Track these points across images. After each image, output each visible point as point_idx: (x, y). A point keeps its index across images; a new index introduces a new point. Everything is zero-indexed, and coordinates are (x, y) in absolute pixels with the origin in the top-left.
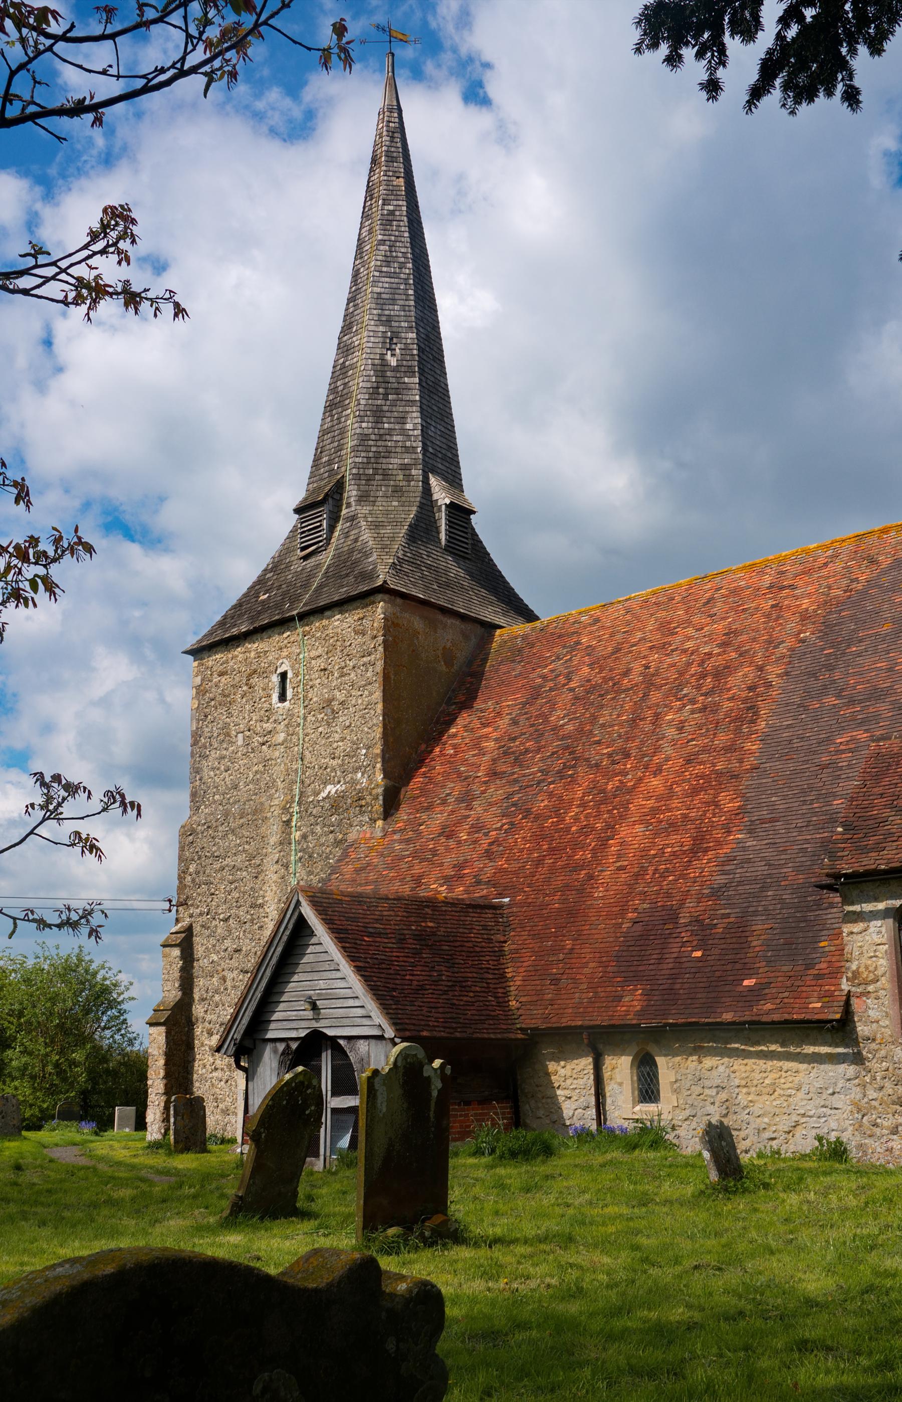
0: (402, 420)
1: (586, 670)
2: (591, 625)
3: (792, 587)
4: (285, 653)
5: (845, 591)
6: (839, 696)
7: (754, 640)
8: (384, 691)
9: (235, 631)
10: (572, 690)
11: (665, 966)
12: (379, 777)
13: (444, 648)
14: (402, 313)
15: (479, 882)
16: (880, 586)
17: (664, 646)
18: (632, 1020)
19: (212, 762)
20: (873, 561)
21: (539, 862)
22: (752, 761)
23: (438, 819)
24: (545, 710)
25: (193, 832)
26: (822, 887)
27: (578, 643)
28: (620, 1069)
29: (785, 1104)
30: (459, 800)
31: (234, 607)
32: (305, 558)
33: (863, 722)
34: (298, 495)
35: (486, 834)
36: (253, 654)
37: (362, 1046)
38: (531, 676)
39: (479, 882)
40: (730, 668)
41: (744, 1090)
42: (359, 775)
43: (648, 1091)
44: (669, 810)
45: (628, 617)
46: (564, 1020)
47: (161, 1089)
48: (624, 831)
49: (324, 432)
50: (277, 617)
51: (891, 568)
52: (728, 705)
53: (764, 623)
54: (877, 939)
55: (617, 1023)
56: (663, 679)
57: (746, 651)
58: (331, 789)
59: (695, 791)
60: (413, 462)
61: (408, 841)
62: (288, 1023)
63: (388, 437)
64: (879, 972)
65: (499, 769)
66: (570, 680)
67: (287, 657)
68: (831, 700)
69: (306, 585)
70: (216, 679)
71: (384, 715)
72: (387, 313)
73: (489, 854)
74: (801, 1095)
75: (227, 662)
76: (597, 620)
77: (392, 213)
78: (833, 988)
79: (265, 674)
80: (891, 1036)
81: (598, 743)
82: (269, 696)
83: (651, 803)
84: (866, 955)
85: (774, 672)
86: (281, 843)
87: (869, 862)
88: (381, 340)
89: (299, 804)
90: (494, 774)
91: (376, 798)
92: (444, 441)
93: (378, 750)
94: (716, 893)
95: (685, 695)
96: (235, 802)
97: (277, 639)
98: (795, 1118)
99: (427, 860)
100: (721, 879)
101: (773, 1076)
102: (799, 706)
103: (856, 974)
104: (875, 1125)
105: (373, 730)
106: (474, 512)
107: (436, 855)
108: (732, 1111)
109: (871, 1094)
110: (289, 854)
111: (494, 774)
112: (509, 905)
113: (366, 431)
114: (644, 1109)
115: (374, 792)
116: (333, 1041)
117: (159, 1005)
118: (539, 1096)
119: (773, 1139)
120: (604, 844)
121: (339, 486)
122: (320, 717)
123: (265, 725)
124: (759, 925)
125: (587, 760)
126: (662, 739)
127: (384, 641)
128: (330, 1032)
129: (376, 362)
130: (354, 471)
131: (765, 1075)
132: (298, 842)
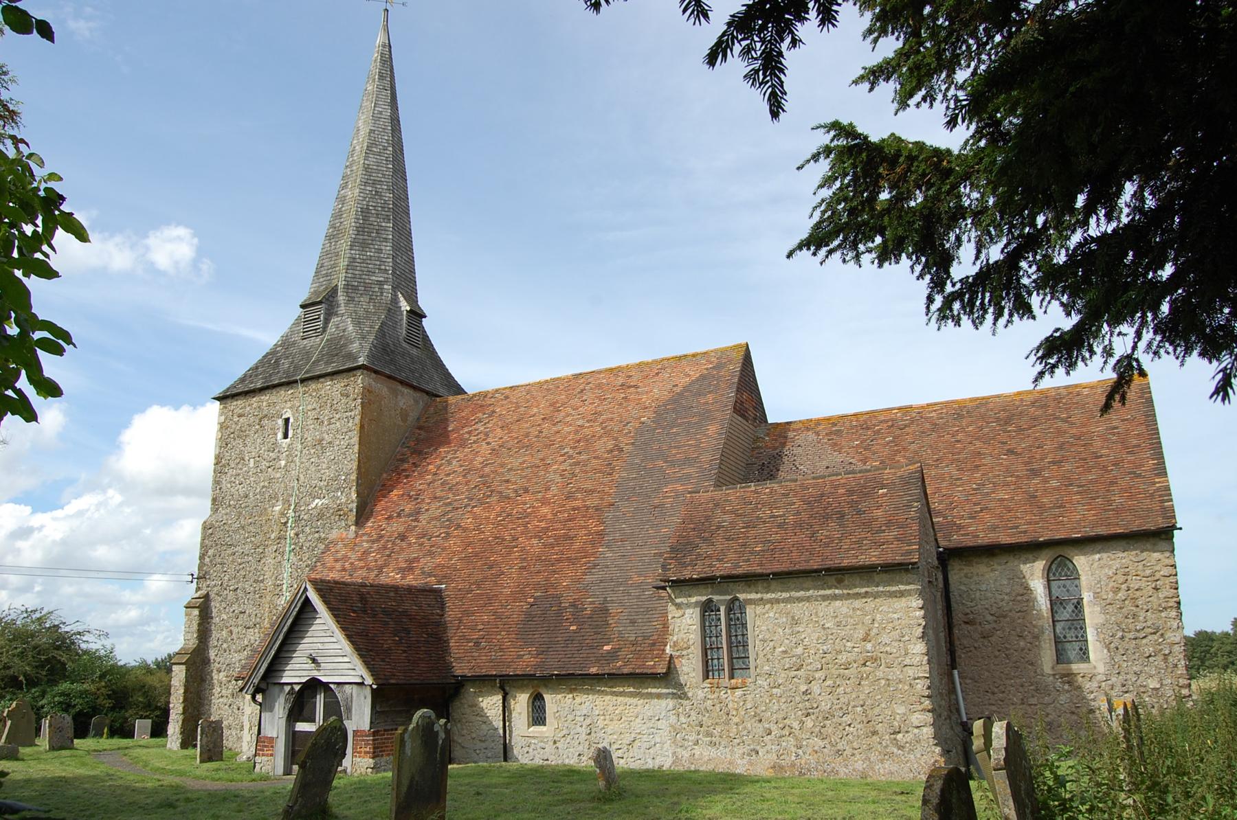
3: (636, 387)
4: (289, 405)
12: (354, 496)
26: (658, 588)
27: (494, 412)
28: (521, 702)
34: (304, 296)
37: (347, 688)
39: (423, 573)
43: (538, 716)
51: (697, 380)
62: (295, 673)
70: (236, 419)
74: (638, 720)
76: (507, 397)
79: (271, 417)
83: (543, 525)
87: (687, 574)
93: (354, 477)
97: (283, 393)
101: (621, 708)
109: (683, 719)
112: (446, 589)
116: (326, 686)
121: (334, 290)
128: (324, 679)
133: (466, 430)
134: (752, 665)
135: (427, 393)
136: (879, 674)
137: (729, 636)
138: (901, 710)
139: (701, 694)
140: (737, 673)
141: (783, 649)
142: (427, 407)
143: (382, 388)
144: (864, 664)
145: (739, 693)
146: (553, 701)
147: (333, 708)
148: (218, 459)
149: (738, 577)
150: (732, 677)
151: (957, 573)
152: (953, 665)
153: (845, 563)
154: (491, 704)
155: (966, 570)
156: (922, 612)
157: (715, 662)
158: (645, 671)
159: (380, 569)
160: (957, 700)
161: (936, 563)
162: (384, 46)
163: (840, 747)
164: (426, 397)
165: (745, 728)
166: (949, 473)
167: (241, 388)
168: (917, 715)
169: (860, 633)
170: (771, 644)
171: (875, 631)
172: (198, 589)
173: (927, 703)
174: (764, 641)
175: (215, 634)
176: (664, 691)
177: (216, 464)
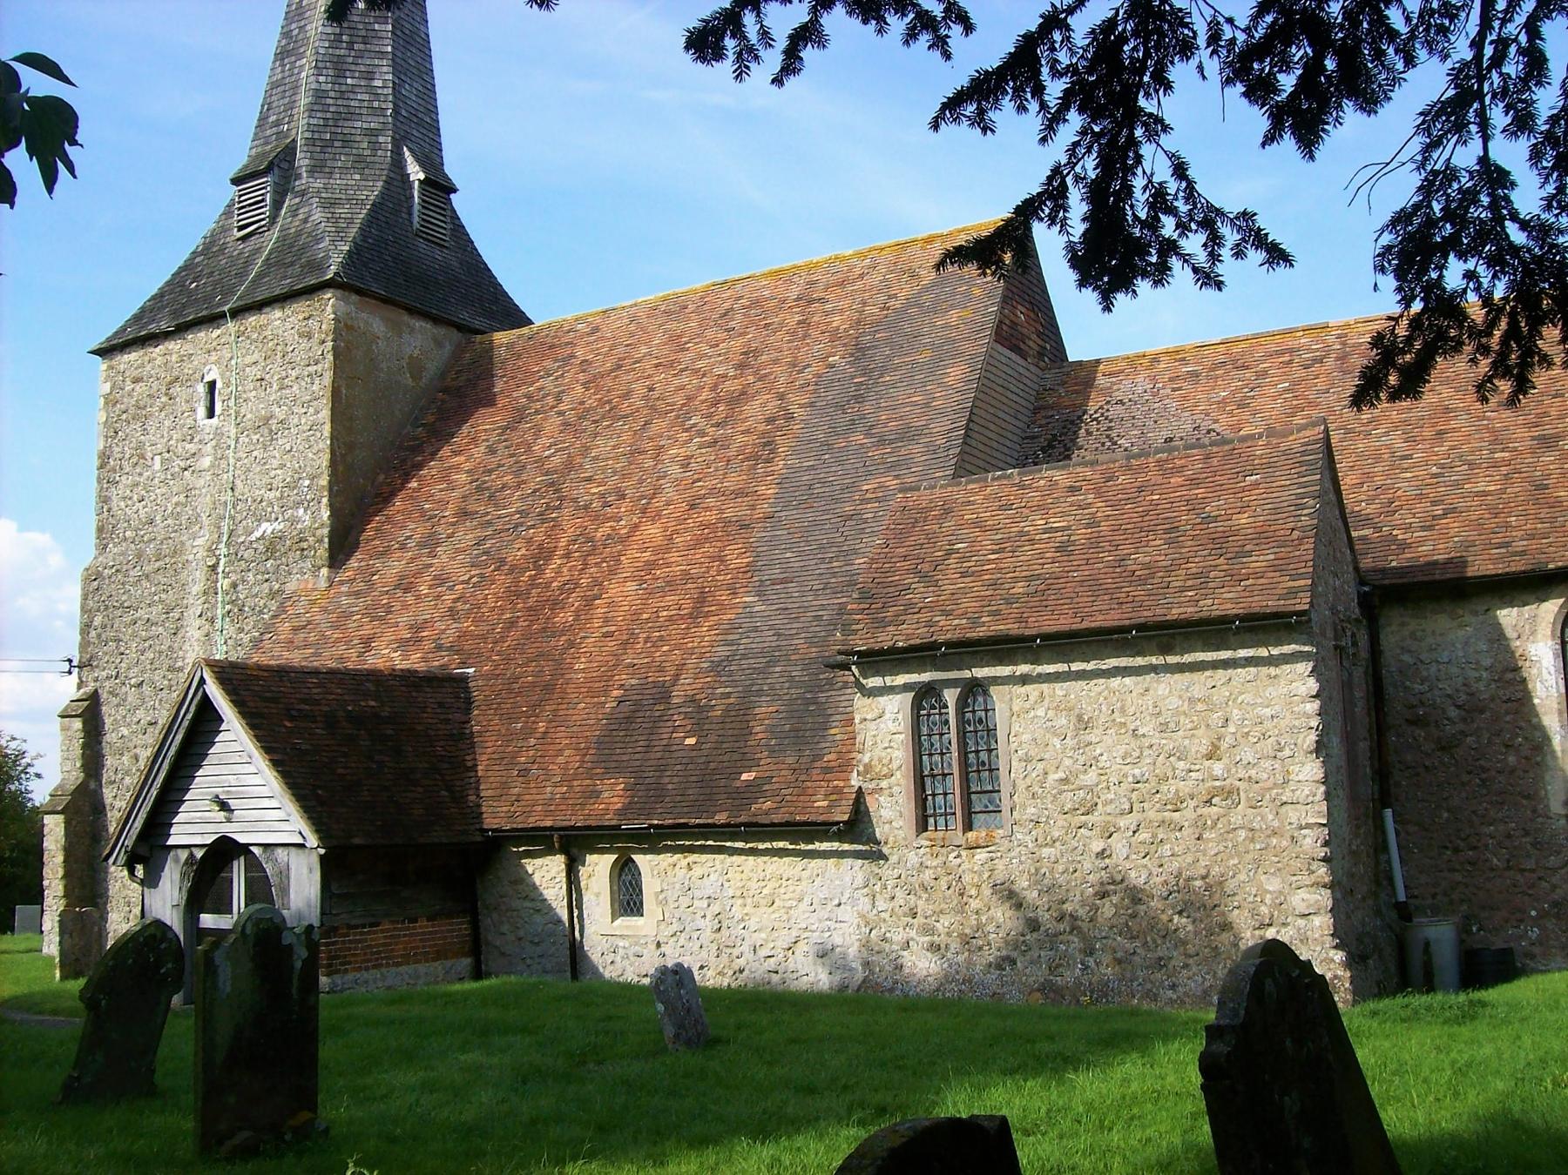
0: (369, 76)
1: (579, 389)
2: (589, 334)
5: (882, 309)
6: (868, 435)
7: (776, 361)
9: (153, 328)
10: (561, 413)
11: (652, 756)
13: (411, 357)
15: (439, 648)
16: (920, 306)
17: (671, 364)
18: (610, 820)
19: (122, 490)
20: (914, 276)
21: (512, 623)
22: (765, 508)
23: (394, 567)
24: (528, 437)
25: (98, 576)
27: (572, 356)
30: (421, 545)
31: (153, 298)
32: (244, 239)
33: (894, 466)
34: (239, 159)
35: (451, 588)
36: (174, 358)
38: (515, 395)
39: (439, 648)
40: (743, 396)
41: (740, 901)
42: (301, 511)
43: (628, 900)
44: (668, 565)
45: (632, 327)
46: (531, 820)
47: (61, 892)
48: (613, 590)
49: (274, 85)
50: (204, 313)
52: (740, 438)
53: (789, 341)
54: (893, 727)
55: (594, 824)
57: (766, 375)
59: (698, 543)
61: (357, 594)
62: (192, 828)
64: (895, 765)
65: (470, 508)
66: (560, 401)
67: (217, 362)
68: (859, 438)
69: (242, 275)
73: (452, 613)
74: (804, 906)
75: (143, 366)
76: (596, 330)
78: (841, 784)
79: (188, 382)
80: (905, 839)
81: (589, 479)
84: (881, 746)
85: (796, 403)
86: (205, 593)
87: (885, 639)
89: (228, 545)
90: (464, 514)
91: (320, 541)
93: (324, 481)
94: (718, 668)
95: (694, 425)
96: (150, 541)
97: (202, 336)
98: (794, 933)
99: (380, 619)
100: (723, 651)
101: (771, 885)
103: (868, 768)
104: (884, 940)
105: (318, 457)
106: (455, 191)
107: (390, 612)
108: (724, 925)
110: (215, 606)
111: (464, 514)
113: (324, 87)
115: (319, 532)
116: (245, 849)
117: (56, 789)
118: (503, 908)
120: (589, 602)
121: (290, 151)
122: (255, 438)
123: (188, 446)
124: (764, 709)
125: (575, 500)
130: (308, 135)
133: (524, 390)
134: (1005, 805)
135: (460, 328)
136: (1236, 818)
137: (964, 754)
138: (1273, 885)
139: (913, 858)
140: (979, 819)
141: (1061, 775)
142: (457, 355)
143: (375, 323)
144: (1209, 802)
145: (981, 855)
146: (656, 870)
147: (259, 887)
150: (968, 827)
151: (1398, 631)
152: (1384, 798)
153: (1175, 613)
154: (546, 873)
155: (1413, 624)
156: (1316, 705)
157: (940, 799)
158: (813, 818)
159: (367, 642)
160: (1389, 862)
161: (1356, 612)
164: (455, 335)
166: (1388, 447)
167: (131, 334)
168: (1302, 894)
169: (1202, 744)
170: (1040, 766)
171: (1229, 740)
172: (80, 685)
173: (1322, 871)
174: (1027, 760)
175: (109, 761)
176: (846, 847)
177: (101, 467)
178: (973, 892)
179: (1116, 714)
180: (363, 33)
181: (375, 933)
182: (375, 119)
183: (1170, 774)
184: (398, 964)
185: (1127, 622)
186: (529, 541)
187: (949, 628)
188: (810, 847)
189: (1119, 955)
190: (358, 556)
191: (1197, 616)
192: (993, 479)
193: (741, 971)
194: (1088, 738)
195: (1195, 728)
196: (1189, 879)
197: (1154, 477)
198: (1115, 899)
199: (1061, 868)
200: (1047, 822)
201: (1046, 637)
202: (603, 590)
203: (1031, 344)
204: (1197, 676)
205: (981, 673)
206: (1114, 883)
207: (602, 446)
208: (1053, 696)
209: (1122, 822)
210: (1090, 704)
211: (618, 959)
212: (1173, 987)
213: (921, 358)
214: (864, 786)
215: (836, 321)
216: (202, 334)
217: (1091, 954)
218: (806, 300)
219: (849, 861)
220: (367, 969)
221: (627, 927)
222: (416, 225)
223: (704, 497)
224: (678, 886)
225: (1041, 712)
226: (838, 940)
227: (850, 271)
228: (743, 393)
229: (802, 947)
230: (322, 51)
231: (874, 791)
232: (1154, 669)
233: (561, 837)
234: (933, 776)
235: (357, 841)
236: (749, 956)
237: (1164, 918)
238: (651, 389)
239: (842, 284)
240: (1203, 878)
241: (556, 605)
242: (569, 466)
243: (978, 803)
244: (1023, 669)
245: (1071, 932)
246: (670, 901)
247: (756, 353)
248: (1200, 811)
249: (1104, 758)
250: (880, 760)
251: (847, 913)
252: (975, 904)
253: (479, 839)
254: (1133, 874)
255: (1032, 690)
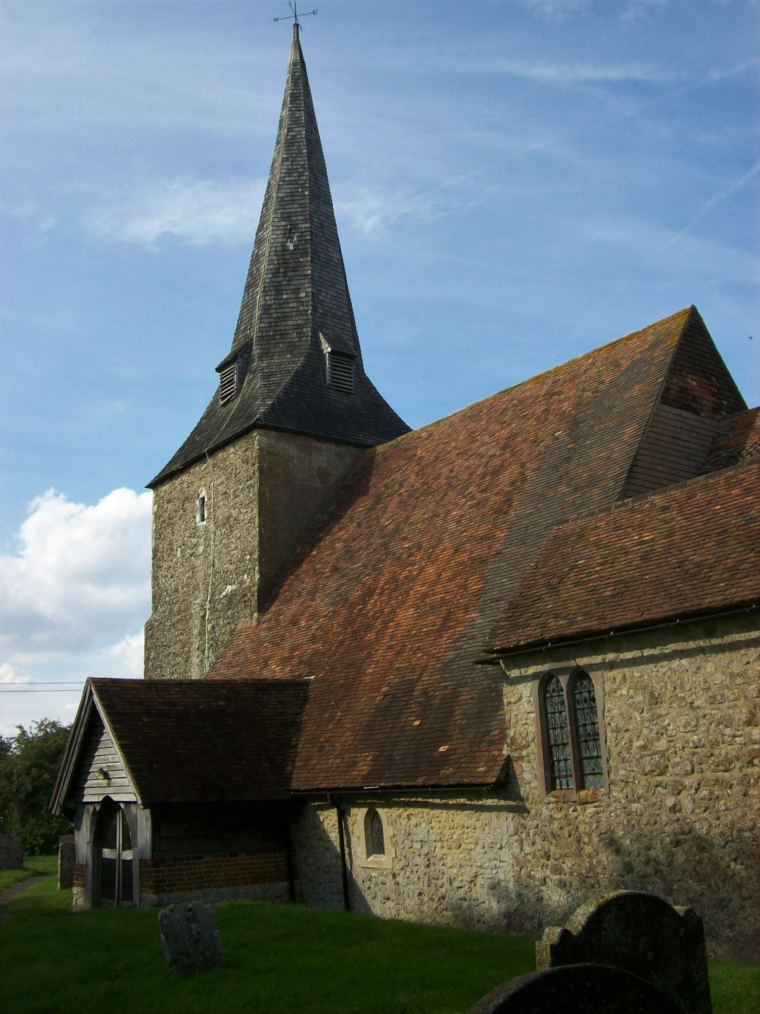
0: (297, 291)
1: (413, 477)
5: (594, 392)
8: (259, 508)
10: (400, 495)
13: (319, 468)
14: (300, 210)
20: (617, 365)
21: (342, 643)
25: (152, 625)
26: (483, 662)
27: (415, 455)
29: (468, 857)
32: (224, 405)
40: (502, 467)
41: (440, 844)
43: (376, 845)
46: (316, 783)
52: (493, 499)
53: (536, 425)
55: (349, 785)
56: (459, 480)
57: (517, 452)
58: (229, 588)
60: (304, 322)
63: (286, 305)
65: (339, 565)
67: (205, 485)
68: (563, 489)
71: (260, 527)
72: (288, 211)
74: (479, 848)
77: (294, 137)
80: (539, 796)
81: (405, 539)
82: (195, 517)
88: (283, 232)
91: (253, 595)
92: (336, 303)
95: (470, 493)
97: (198, 469)
98: (474, 870)
101: (459, 831)
102: (540, 496)
103: (513, 739)
104: (530, 876)
111: (335, 570)
113: (269, 302)
114: (376, 859)
119: (461, 887)
120: (385, 626)
124: (466, 694)
126: (444, 532)
127: (259, 468)
129: (279, 249)
131: (453, 831)
132: (210, 633)
134: (605, 767)
135: (357, 445)
139: (546, 813)
141: (641, 743)
143: (290, 449)
144: (750, 763)
145: (590, 810)
148: (155, 551)
149: (572, 637)
153: (708, 602)
154: (329, 819)
159: (266, 663)
162: (294, 64)
163: (723, 894)
164: (354, 450)
165: (599, 862)
170: (627, 735)
174: (617, 731)
176: (502, 802)
178: (586, 840)
179: (678, 691)
180: (293, 265)
181: (200, 863)
182: (302, 318)
183: (720, 739)
184: (219, 886)
185: (671, 613)
186: (364, 584)
187: (556, 627)
188: (480, 803)
189: (691, 895)
190: (277, 603)
191: (721, 604)
192: (616, 507)
193: (444, 898)
194: (658, 711)
195: (736, 699)
196: (740, 830)
197: (721, 491)
198: (686, 847)
199: (644, 820)
200: (633, 783)
201: (617, 629)
202: (395, 616)
203: (704, 402)
204: (736, 655)
205: (583, 661)
206: (683, 833)
207: (418, 515)
208: (633, 677)
209: (687, 782)
210: (658, 683)
211: (372, 886)
212: (731, 926)
213: (610, 424)
214: (512, 754)
215: (565, 406)
216: (197, 468)
217: (670, 894)
218: (550, 394)
219: (504, 814)
220: (191, 889)
221: (376, 862)
222: (328, 382)
223: (464, 543)
224: (403, 832)
225: (624, 692)
226: (501, 876)
227: (579, 369)
228: (502, 466)
229: (480, 881)
230: (267, 281)
231: (521, 758)
232: (702, 650)
233: (331, 796)
234: (557, 746)
235: (174, 800)
236: (447, 886)
237: (723, 864)
238: (451, 471)
239: (572, 380)
240: (752, 829)
241: (368, 628)
242: (396, 530)
243: (588, 766)
244: (611, 656)
245: (656, 873)
246: (399, 844)
247: (516, 436)
248: (745, 771)
249: (671, 727)
250: (520, 734)
251: (506, 855)
252: (588, 849)
253: (286, 797)
254: (697, 826)
255: (617, 673)
